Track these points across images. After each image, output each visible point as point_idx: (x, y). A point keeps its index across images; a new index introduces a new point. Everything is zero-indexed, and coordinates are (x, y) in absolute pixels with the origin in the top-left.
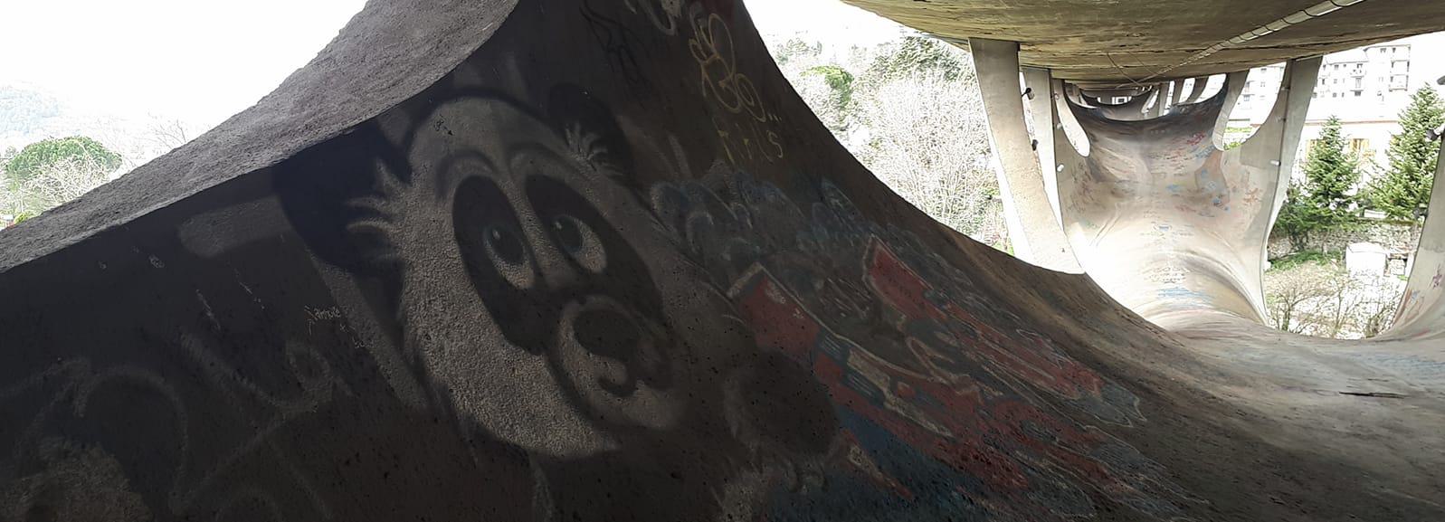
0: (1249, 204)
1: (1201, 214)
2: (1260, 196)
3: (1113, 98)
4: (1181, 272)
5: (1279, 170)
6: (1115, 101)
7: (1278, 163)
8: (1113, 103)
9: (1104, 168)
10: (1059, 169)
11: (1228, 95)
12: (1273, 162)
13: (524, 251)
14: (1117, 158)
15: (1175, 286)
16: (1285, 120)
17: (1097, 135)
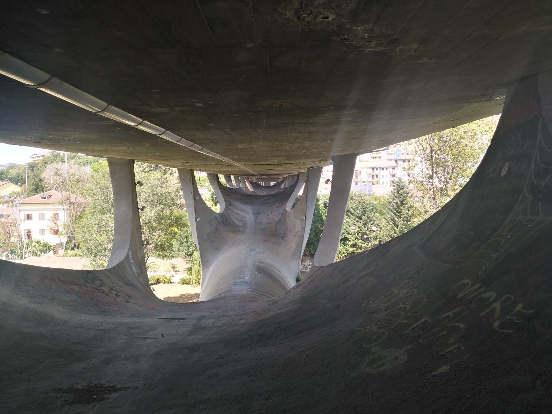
0: (295, 238)
1: (273, 243)
2: (299, 234)
3: (271, 183)
4: (251, 273)
5: (305, 220)
7: (304, 218)
8: (271, 185)
9: (231, 219)
10: (198, 220)
11: (298, 183)
12: (302, 217)
13: (439, 355)
14: (240, 214)
15: (243, 280)
16: (307, 196)
17: (233, 202)
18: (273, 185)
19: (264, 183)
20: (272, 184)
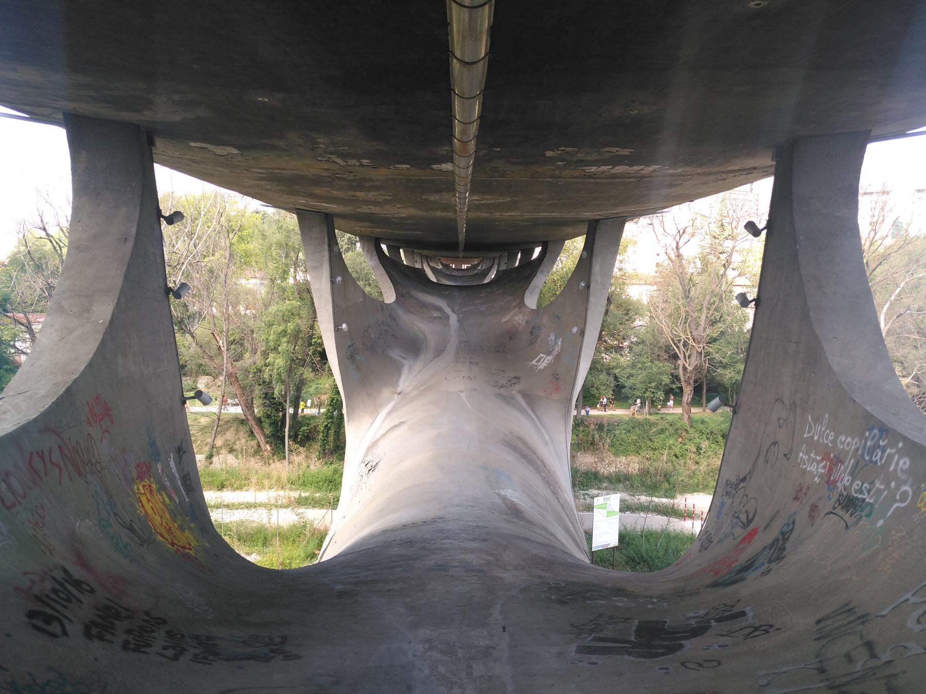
6: (464, 267)
18: (465, 268)
19: (454, 265)
20: (464, 267)
